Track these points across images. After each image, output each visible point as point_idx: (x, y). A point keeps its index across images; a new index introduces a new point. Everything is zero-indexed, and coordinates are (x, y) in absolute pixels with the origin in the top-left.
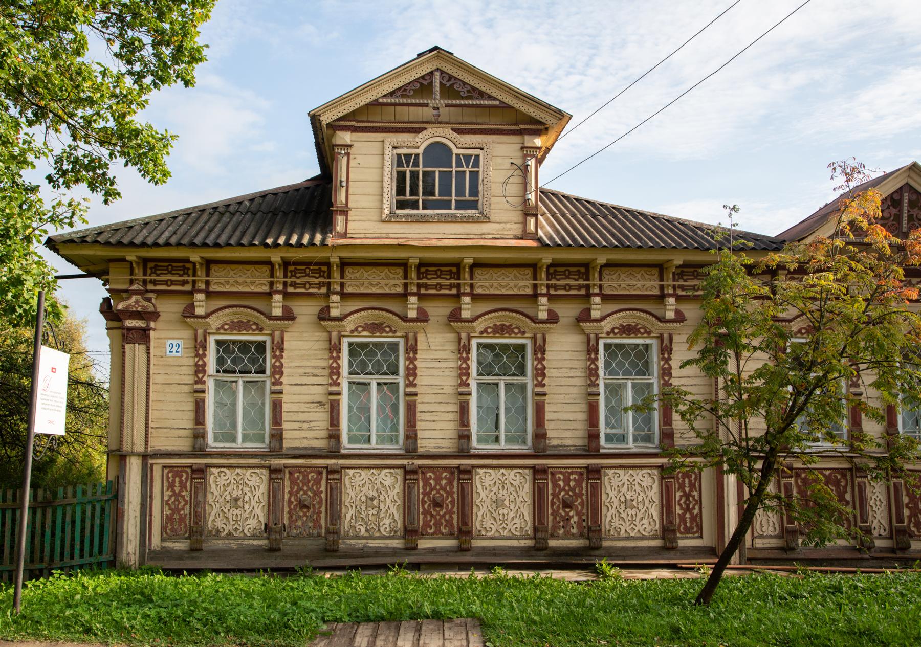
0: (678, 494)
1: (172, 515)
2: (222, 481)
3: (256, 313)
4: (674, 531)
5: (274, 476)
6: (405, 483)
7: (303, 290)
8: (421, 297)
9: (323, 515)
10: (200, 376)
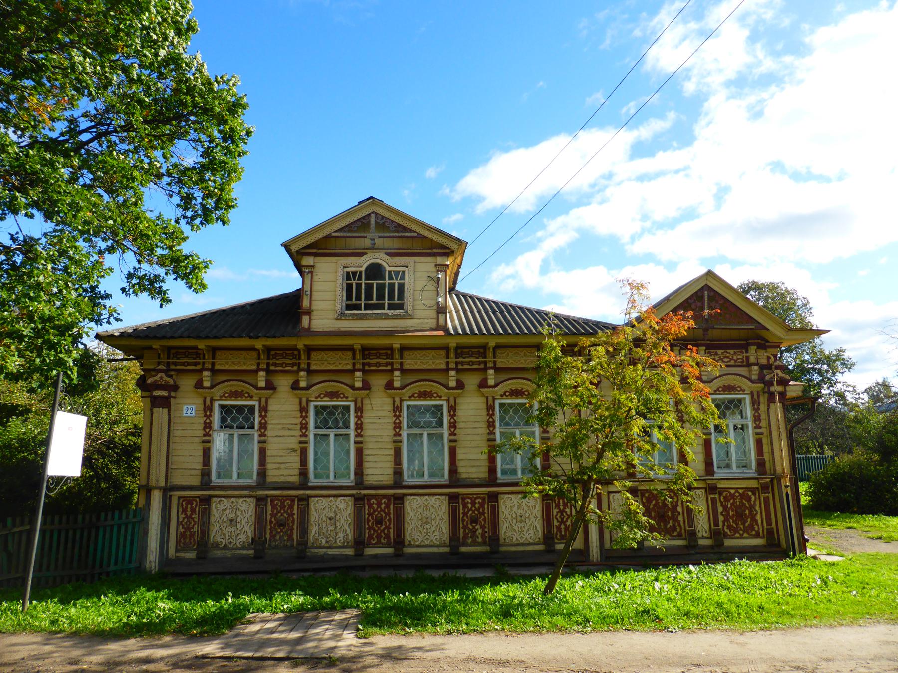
0: (555, 511)
1: (184, 532)
2: (221, 507)
3: (246, 385)
4: (553, 539)
5: (259, 503)
6: (354, 507)
7: (280, 368)
8: (458, 371)
9: (295, 532)
10: (207, 430)
